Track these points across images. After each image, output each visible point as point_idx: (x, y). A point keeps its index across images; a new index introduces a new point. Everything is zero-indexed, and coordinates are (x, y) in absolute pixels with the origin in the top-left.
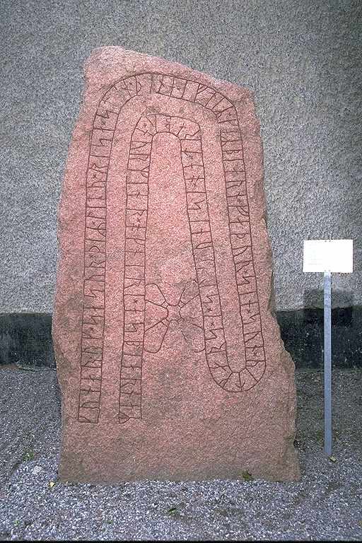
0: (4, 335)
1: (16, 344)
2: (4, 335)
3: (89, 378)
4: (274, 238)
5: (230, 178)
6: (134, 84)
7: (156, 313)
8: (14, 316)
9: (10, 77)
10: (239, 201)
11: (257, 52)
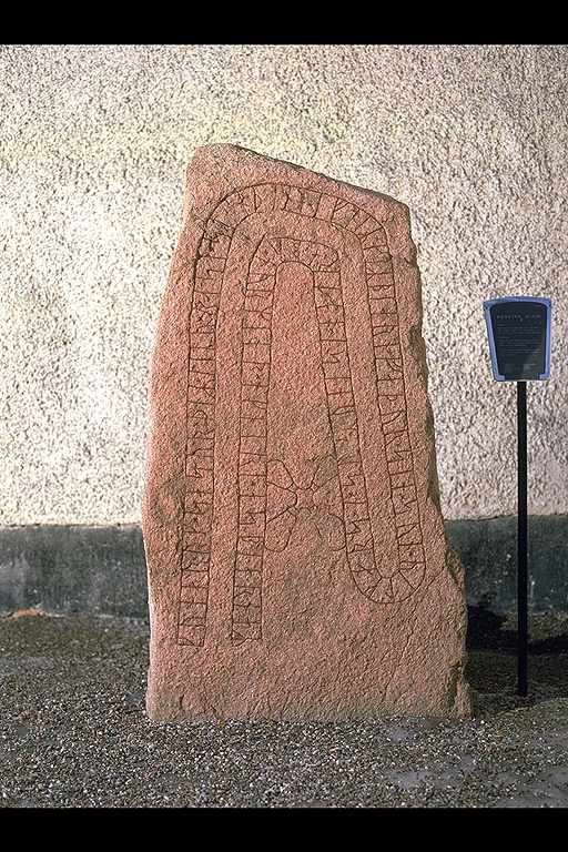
0: (17, 560)
1: (37, 574)
2: (17, 560)
3: (192, 585)
4: (455, 403)
5: (377, 321)
6: (252, 197)
7: (279, 500)
8: (36, 530)
9: (34, 144)
10: (390, 352)
11: (427, 113)
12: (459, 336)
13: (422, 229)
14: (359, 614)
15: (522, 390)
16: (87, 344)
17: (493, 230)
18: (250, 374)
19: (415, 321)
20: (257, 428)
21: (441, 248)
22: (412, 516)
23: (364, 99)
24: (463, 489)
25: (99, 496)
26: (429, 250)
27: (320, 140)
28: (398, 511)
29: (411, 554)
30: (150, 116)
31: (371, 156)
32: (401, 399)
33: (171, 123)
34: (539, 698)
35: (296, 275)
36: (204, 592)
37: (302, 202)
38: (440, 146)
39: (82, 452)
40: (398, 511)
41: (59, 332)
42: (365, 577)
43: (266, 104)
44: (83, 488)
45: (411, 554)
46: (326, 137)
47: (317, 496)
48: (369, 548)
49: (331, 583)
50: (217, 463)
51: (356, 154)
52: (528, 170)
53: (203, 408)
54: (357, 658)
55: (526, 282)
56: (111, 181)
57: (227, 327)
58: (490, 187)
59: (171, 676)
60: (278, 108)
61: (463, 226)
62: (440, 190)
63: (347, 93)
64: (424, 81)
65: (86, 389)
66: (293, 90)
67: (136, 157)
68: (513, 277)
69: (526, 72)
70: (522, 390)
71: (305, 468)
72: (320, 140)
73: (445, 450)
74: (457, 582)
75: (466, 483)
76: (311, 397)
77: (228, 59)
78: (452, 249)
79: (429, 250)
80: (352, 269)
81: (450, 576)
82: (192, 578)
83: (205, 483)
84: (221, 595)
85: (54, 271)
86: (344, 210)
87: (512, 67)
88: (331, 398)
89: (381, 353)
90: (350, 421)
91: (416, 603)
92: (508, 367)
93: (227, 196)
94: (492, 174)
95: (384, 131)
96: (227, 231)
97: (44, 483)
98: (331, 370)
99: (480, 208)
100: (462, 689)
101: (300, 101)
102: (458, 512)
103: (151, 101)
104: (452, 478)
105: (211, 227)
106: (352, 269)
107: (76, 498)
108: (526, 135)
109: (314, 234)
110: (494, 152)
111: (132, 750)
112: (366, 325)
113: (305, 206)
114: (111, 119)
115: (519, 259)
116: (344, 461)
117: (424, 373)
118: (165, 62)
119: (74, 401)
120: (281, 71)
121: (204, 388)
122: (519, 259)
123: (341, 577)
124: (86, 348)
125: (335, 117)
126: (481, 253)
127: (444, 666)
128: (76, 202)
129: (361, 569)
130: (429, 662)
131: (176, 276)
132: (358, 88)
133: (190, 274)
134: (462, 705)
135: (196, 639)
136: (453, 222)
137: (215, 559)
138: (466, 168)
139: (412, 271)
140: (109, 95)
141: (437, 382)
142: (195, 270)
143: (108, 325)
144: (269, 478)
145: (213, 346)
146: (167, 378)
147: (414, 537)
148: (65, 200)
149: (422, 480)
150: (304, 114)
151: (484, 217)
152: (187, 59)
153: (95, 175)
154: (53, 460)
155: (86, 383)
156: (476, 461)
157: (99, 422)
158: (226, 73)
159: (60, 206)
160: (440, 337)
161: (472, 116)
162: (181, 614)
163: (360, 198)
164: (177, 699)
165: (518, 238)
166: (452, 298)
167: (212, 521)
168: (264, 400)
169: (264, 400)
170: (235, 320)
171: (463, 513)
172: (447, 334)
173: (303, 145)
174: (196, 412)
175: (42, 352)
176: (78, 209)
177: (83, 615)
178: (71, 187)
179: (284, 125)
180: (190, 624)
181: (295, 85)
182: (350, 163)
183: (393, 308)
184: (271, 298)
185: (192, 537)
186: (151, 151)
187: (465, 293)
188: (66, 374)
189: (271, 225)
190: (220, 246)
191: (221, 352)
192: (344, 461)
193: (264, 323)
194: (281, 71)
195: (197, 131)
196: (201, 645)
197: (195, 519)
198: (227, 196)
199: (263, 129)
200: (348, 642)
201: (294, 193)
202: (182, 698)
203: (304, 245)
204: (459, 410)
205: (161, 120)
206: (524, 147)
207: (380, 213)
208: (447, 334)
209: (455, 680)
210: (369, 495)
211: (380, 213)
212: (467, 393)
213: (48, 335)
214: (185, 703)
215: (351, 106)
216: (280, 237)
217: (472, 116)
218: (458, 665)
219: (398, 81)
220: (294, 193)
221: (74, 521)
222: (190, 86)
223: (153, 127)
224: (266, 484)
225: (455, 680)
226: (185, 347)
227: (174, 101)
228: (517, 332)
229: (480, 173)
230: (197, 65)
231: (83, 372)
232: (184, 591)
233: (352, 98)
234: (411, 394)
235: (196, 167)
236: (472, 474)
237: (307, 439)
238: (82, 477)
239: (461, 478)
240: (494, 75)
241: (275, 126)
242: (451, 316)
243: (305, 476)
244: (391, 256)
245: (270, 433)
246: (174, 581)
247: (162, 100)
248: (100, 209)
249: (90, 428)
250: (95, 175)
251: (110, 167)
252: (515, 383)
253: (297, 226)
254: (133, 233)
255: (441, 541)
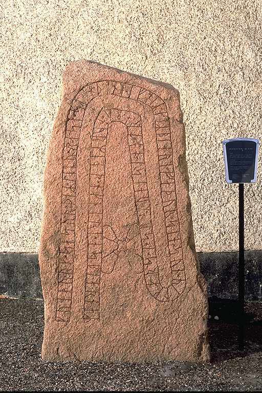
3: (64, 290)
5: (161, 152)
7: (109, 246)
10: (168, 169)
12: (206, 157)
13: (202, 99)
14: (151, 307)
15: (241, 188)
16: (30, 161)
17: (240, 99)
18: (94, 181)
19: (181, 153)
20: (97, 209)
21: (212, 109)
22: (178, 256)
23: (172, 33)
24: (223, 236)
25: (36, 237)
26: (206, 110)
27: (149, 53)
28: (171, 253)
29: (178, 276)
30: (62, 43)
31: (175, 61)
32: (174, 194)
33: (73, 46)
34: (250, 352)
35: (119, 129)
36: (70, 294)
37: (122, 90)
38: (212, 55)
39: (27, 216)
40: (171, 253)
41: (16, 154)
42: (154, 287)
43: (121, 36)
44: (28, 234)
45: (178, 276)
46: (152, 52)
47: (129, 245)
48: (156, 272)
49: (136, 290)
50: (77, 227)
51: (167, 61)
52: (258, 67)
53: (70, 198)
54: (149, 330)
55: (257, 127)
56: (42, 77)
57: (83, 155)
58: (238, 77)
59: (52, 337)
60: (127, 37)
61: (224, 98)
62: (212, 79)
63: (163, 29)
64: (203, 22)
65: (29, 183)
66: (135, 28)
67: (54, 64)
68: (251, 124)
69: (258, 16)
70: (241, 188)
71: (123, 230)
72: (149, 53)
73: (214, 215)
74: (203, 291)
75: (225, 232)
76: (126, 192)
77: (101, 12)
78: (218, 110)
79: (206, 110)
80: (148, 125)
81: (199, 288)
82: (64, 287)
83: (70, 237)
84: (78, 296)
85: (13, 123)
86: (144, 94)
87: (251, 13)
88: (136, 193)
89: (163, 169)
90: (146, 205)
91: (181, 301)
92: (235, 176)
93: (83, 87)
94: (239, 70)
95: (182, 48)
96: (83, 106)
97: (8, 231)
98: (137, 178)
99: (233, 88)
100: (205, 348)
101: (139, 33)
102: (221, 248)
103: (62, 35)
104: (218, 230)
105: (75, 104)
106: (148, 125)
107: (25, 239)
108: (258, 49)
109: (128, 106)
110: (240, 58)
111: (26, 377)
112: (155, 155)
113: (124, 92)
114: (42, 45)
115: (254, 114)
116: (144, 226)
117: (186, 180)
118: (69, 15)
119: (23, 189)
120: (129, 18)
121: (70, 188)
122: (254, 114)
123: (141, 286)
124: (30, 162)
125: (157, 42)
126: (233, 112)
127: (195, 335)
128: (24, 88)
129: (152, 283)
130: (188, 333)
131: (57, 129)
132: (168, 26)
133: (64, 129)
134: (205, 355)
135: (65, 319)
136: (219, 95)
137: (75, 277)
138: (226, 68)
139: (181, 126)
140: (41, 33)
141: (210, 180)
142: (66, 126)
143: (40, 151)
144: (104, 235)
145: (75, 166)
146: (51, 183)
147: (180, 267)
148: (19, 87)
149: (185, 236)
150: (140, 40)
151: (235, 92)
152: (80, 13)
153: (33, 74)
154: (13, 220)
155: (30, 180)
156: (230, 221)
157: (36, 200)
158: (100, 20)
159: (17, 90)
160: (212, 156)
161: (229, 40)
162: (58, 305)
163: (153, 87)
164: (56, 349)
165: (253, 104)
166: (218, 136)
167: (74, 257)
168: (101, 194)
169: (101, 194)
170: (87, 153)
171: (223, 249)
172: (215, 154)
173: (140, 56)
174: (66, 200)
175: (8, 164)
176: (25, 91)
177: (28, 299)
178: (22, 80)
179: (130, 46)
180: (64, 309)
181: (136, 25)
182: (164, 65)
183: (170, 146)
184: (105, 140)
185: (63, 266)
186: (62, 61)
187: (225, 133)
188: (20, 176)
189: (106, 102)
190: (79, 114)
191: (79, 169)
192: (144, 226)
193: (102, 154)
194: (129, 18)
195: (85, 50)
196: (68, 321)
197: (65, 256)
198: (83, 87)
199: (119, 49)
200: (144, 322)
201: (118, 85)
202: (58, 349)
203: (123, 113)
204: (222, 194)
205: (67, 45)
206: (256, 55)
207: (164, 95)
208: (215, 154)
209: (201, 343)
210: (157, 245)
211: (164, 95)
212: (226, 185)
213: (11, 156)
214: (60, 351)
215: (165, 36)
216: (110, 108)
217: (229, 40)
218: (203, 335)
219: (190, 22)
220: (118, 85)
221: (24, 251)
222: (82, 26)
223: (63, 49)
224: (103, 238)
225: (201, 343)
226: (61, 167)
227: (74, 34)
228: (240, 157)
229: (233, 69)
230: (85, 15)
231: (28, 174)
232: (60, 293)
233: (165, 31)
234: (179, 191)
235: (68, 73)
236: (214, 233)
237: (124, 215)
238: (27, 228)
239: (222, 230)
240: (241, 17)
241: (126, 47)
242: (218, 145)
243: (122, 234)
244: (169, 118)
245: (105, 212)
246: (54, 288)
247: (68, 34)
248: (36, 91)
249: (31, 203)
250: (33, 74)
251: (41, 70)
252: (238, 184)
253: (119, 102)
254: (53, 103)
255: (194, 269)
